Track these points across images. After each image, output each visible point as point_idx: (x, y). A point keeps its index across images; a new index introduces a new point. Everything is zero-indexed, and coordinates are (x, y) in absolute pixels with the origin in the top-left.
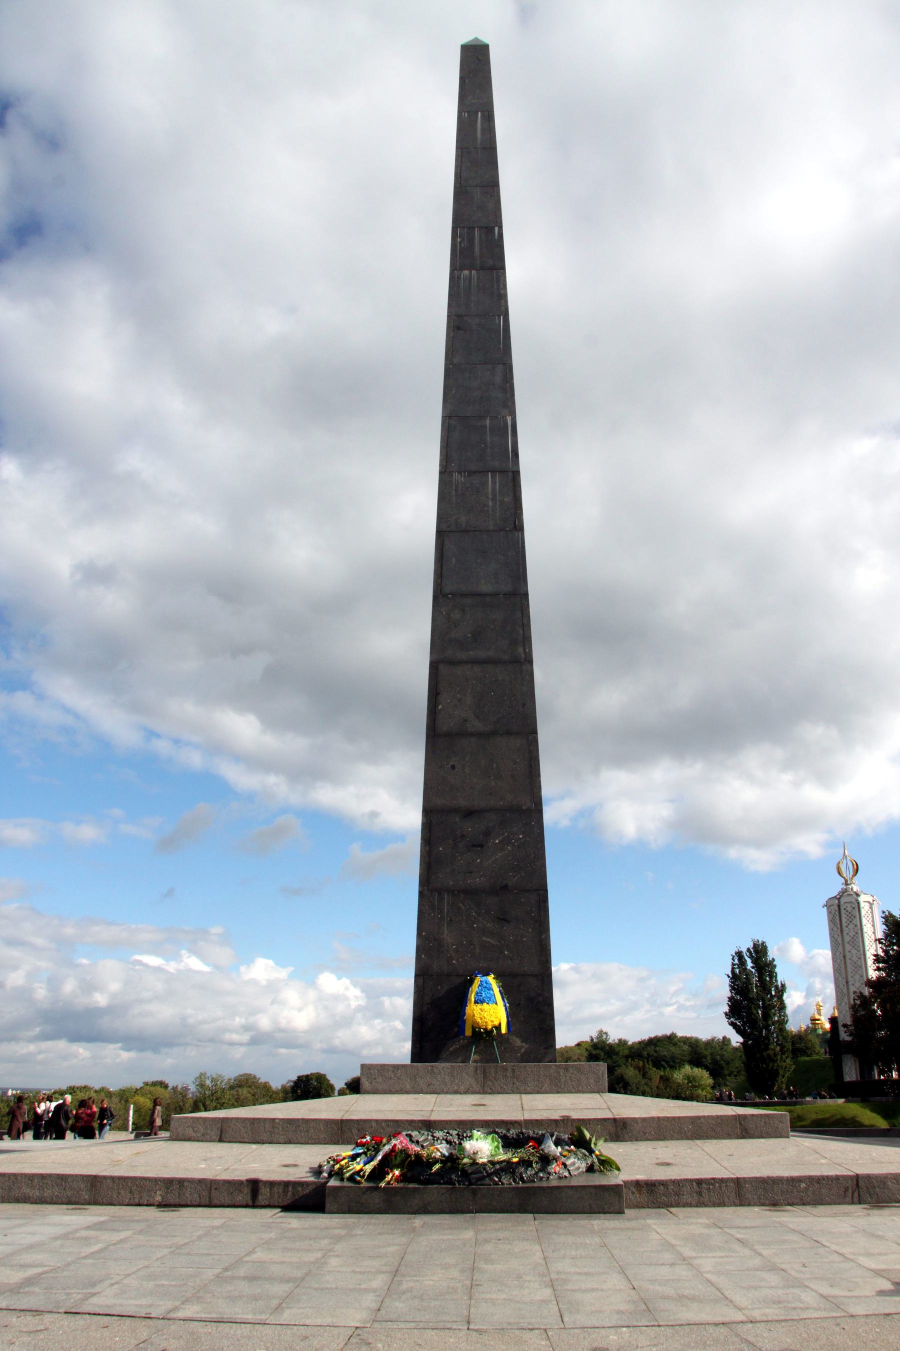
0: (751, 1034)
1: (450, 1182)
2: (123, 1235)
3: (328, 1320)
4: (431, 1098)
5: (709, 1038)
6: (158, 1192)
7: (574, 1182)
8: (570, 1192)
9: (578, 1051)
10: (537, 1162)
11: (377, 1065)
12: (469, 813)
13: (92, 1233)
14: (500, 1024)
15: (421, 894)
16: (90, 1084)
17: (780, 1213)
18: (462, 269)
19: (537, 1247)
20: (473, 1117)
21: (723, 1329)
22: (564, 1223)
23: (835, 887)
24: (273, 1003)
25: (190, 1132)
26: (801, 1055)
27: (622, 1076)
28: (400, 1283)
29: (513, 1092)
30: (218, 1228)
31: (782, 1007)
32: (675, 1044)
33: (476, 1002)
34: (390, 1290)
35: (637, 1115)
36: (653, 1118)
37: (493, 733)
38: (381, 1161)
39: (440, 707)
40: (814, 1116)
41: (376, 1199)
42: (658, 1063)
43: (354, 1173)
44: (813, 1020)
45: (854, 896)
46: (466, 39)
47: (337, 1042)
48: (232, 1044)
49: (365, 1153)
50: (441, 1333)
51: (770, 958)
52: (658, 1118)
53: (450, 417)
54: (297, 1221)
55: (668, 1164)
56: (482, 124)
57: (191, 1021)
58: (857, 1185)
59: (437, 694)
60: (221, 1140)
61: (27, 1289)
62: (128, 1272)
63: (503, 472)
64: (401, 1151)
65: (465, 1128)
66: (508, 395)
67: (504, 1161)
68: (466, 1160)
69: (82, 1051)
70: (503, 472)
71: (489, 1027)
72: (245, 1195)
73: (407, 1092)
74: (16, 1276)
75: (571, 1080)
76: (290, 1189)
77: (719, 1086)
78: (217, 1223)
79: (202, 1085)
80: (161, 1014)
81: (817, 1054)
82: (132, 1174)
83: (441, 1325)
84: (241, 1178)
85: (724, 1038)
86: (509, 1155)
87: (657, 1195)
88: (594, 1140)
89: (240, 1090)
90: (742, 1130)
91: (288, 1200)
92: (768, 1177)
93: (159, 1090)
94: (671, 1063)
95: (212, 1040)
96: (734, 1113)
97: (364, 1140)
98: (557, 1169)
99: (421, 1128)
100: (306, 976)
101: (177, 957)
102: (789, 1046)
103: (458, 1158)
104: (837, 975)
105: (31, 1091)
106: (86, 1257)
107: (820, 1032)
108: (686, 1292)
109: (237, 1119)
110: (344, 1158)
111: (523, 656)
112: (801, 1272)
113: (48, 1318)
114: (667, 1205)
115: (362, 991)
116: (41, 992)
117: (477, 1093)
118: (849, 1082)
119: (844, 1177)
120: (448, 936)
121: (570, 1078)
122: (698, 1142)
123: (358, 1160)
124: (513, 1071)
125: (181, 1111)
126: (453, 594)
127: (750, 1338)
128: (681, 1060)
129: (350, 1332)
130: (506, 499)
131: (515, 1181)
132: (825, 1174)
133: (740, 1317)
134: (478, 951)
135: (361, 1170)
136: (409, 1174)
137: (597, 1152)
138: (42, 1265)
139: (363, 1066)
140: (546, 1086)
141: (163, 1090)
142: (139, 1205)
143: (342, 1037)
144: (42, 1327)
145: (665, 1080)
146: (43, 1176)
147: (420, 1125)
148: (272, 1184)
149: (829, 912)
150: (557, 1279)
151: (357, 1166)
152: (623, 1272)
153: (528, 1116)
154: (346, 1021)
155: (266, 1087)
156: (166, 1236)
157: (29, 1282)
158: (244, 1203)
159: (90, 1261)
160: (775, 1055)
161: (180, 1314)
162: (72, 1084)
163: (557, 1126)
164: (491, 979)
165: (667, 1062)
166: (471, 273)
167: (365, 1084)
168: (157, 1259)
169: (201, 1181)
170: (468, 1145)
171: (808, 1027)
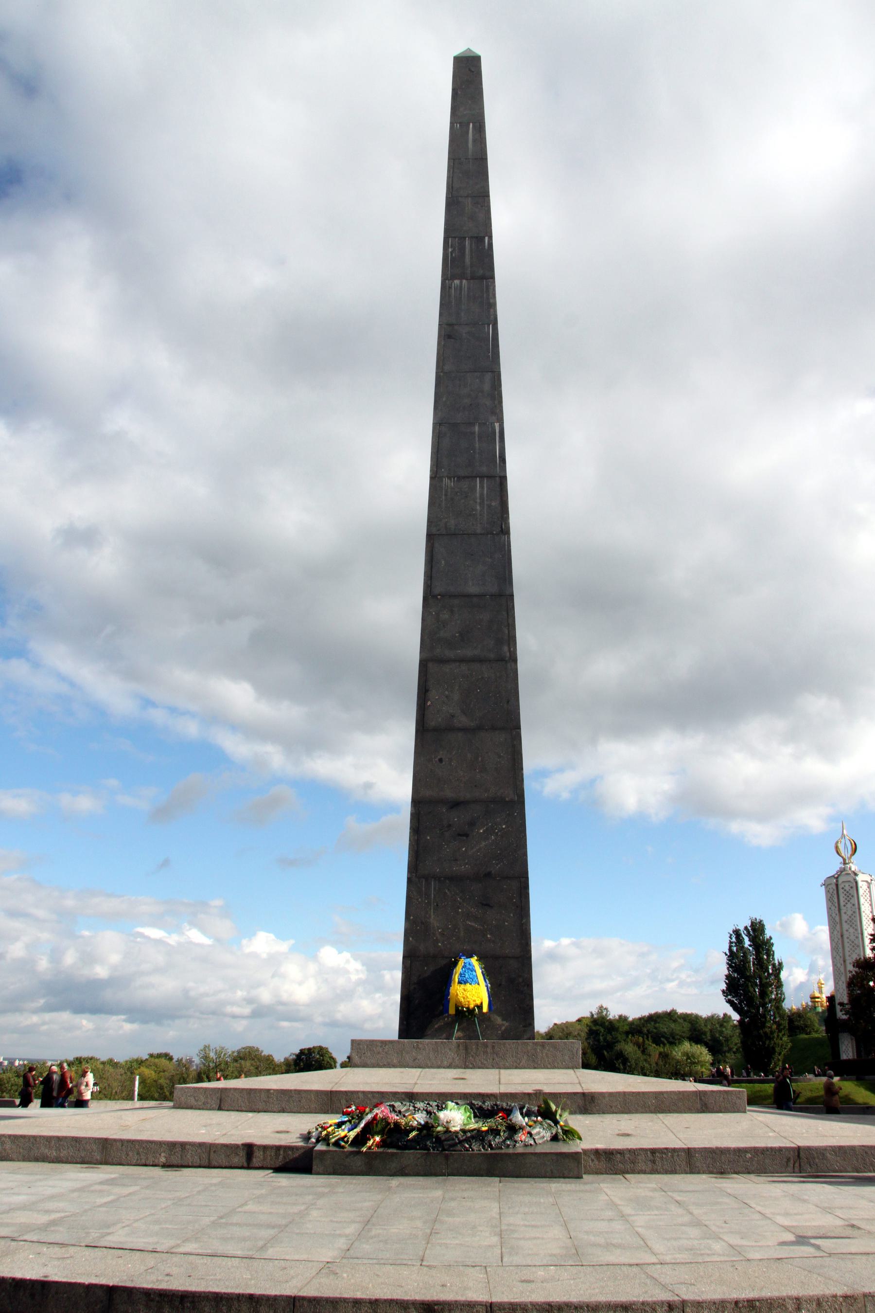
0: (748, 1011)
1: (426, 1148)
2: (132, 1189)
3: (304, 1257)
4: (416, 1072)
5: (710, 1015)
6: (163, 1154)
7: (539, 1150)
8: (534, 1158)
9: (579, 1027)
10: (504, 1131)
11: (366, 1041)
12: (455, 804)
13: (105, 1187)
14: (482, 1003)
15: (410, 881)
16: (97, 1056)
17: (728, 1180)
18: (453, 277)
19: (497, 1205)
20: (448, 1089)
21: (635, 1269)
22: (525, 1185)
23: (833, 866)
24: (273, 976)
25: (192, 1101)
26: (800, 1033)
27: (621, 1052)
28: (370, 1230)
29: (493, 1067)
30: (215, 1185)
31: (779, 985)
32: (675, 1021)
33: (459, 983)
34: (359, 1236)
35: (604, 1090)
36: (619, 1093)
37: (480, 728)
38: (363, 1129)
39: (429, 703)
40: (809, 1094)
41: (358, 1162)
42: (658, 1039)
43: (339, 1139)
44: (813, 998)
45: (852, 875)
46: (458, 50)
47: (339, 1016)
48: (234, 1016)
49: (350, 1121)
50: (398, 1267)
51: (767, 936)
52: (624, 1093)
53: (440, 424)
54: (285, 1180)
55: (628, 1135)
56: (473, 136)
57: (192, 994)
58: (799, 1156)
59: (427, 691)
60: (220, 1109)
61: (52, 1228)
62: (137, 1218)
63: (490, 477)
64: (382, 1119)
65: (442, 1099)
66: (496, 402)
67: (474, 1130)
68: (439, 1129)
69: (86, 1022)
70: (490, 477)
71: (472, 1006)
72: (241, 1159)
73: (394, 1066)
74: (44, 1219)
75: (548, 1057)
76: (282, 1152)
77: (719, 1063)
78: (215, 1181)
79: (206, 1057)
80: (163, 987)
81: (816, 1032)
82: (139, 1138)
83: (399, 1262)
84: (237, 1143)
85: (725, 1015)
86: (480, 1124)
87: (614, 1162)
88: (559, 1112)
89: (243, 1062)
90: (702, 1105)
91: (279, 1163)
92: (717, 1148)
93: (164, 1062)
94: (671, 1040)
95: (214, 1013)
96: (694, 1089)
97: (350, 1110)
98: (523, 1137)
99: (404, 1100)
100: (307, 949)
101: (178, 930)
102: (785, 1023)
103: (433, 1126)
104: (835, 953)
105: (38, 1061)
106: (100, 1206)
107: (820, 1009)
108: (615, 1241)
109: (235, 1089)
110: (331, 1126)
111: (508, 654)
112: (722, 1228)
113: (72, 1250)
114: (623, 1172)
115: (363, 965)
116: (43, 964)
117: (459, 1068)
118: (846, 1060)
119: (787, 1149)
120: (434, 921)
121: (547, 1054)
122: (661, 1115)
123: (343, 1127)
124: (493, 1047)
125: (185, 1082)
126: (443, 596)
127: (655, 1275)
128: (681, 1036)
129: (321, 1265)
130: (493, 504)
131: (484, 1147)
132: (769, 1145)
133: (654, 1259)
134: (462, 934)
135: (346, 1136)
136: (389, 1140)
137: (562, 1123)
138: (63, 1211)
139: (353, 1041)
140: (524, 1061)
141: (168, 1062)
142: (146, 1165)
143: (343, 1010)
144: (68, 1255)
145: (664, 1056)
146: (59, 1139)
147: (403, 1096)
148: (265, 1148)
149: (827, 892)
150: (506, 1230)
151: (342, 1133)
152: (565, 1225)
153: (503, 1089)
154: (346, 995)
155: (269, 1059)
156: (170, 1191)
157: (53, 1223)
158: (241, 1165)
159: (104, 1209)
160: (772, 1032)
161: (181, 1250)
162: (78, 1055)
163: (530, 1099)
164: (474, 961)
165: (667, 1039)
166: (461, 283)
167: (356, 1059)
168: (162, 1209)
169: (201, 1145)
170: (443, 1115)
171: (807, 1006)
